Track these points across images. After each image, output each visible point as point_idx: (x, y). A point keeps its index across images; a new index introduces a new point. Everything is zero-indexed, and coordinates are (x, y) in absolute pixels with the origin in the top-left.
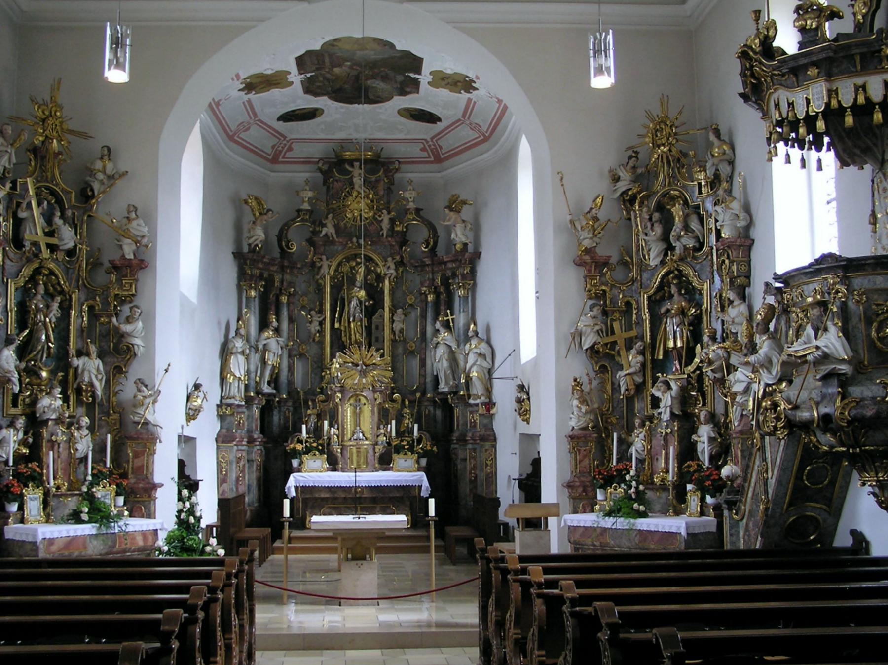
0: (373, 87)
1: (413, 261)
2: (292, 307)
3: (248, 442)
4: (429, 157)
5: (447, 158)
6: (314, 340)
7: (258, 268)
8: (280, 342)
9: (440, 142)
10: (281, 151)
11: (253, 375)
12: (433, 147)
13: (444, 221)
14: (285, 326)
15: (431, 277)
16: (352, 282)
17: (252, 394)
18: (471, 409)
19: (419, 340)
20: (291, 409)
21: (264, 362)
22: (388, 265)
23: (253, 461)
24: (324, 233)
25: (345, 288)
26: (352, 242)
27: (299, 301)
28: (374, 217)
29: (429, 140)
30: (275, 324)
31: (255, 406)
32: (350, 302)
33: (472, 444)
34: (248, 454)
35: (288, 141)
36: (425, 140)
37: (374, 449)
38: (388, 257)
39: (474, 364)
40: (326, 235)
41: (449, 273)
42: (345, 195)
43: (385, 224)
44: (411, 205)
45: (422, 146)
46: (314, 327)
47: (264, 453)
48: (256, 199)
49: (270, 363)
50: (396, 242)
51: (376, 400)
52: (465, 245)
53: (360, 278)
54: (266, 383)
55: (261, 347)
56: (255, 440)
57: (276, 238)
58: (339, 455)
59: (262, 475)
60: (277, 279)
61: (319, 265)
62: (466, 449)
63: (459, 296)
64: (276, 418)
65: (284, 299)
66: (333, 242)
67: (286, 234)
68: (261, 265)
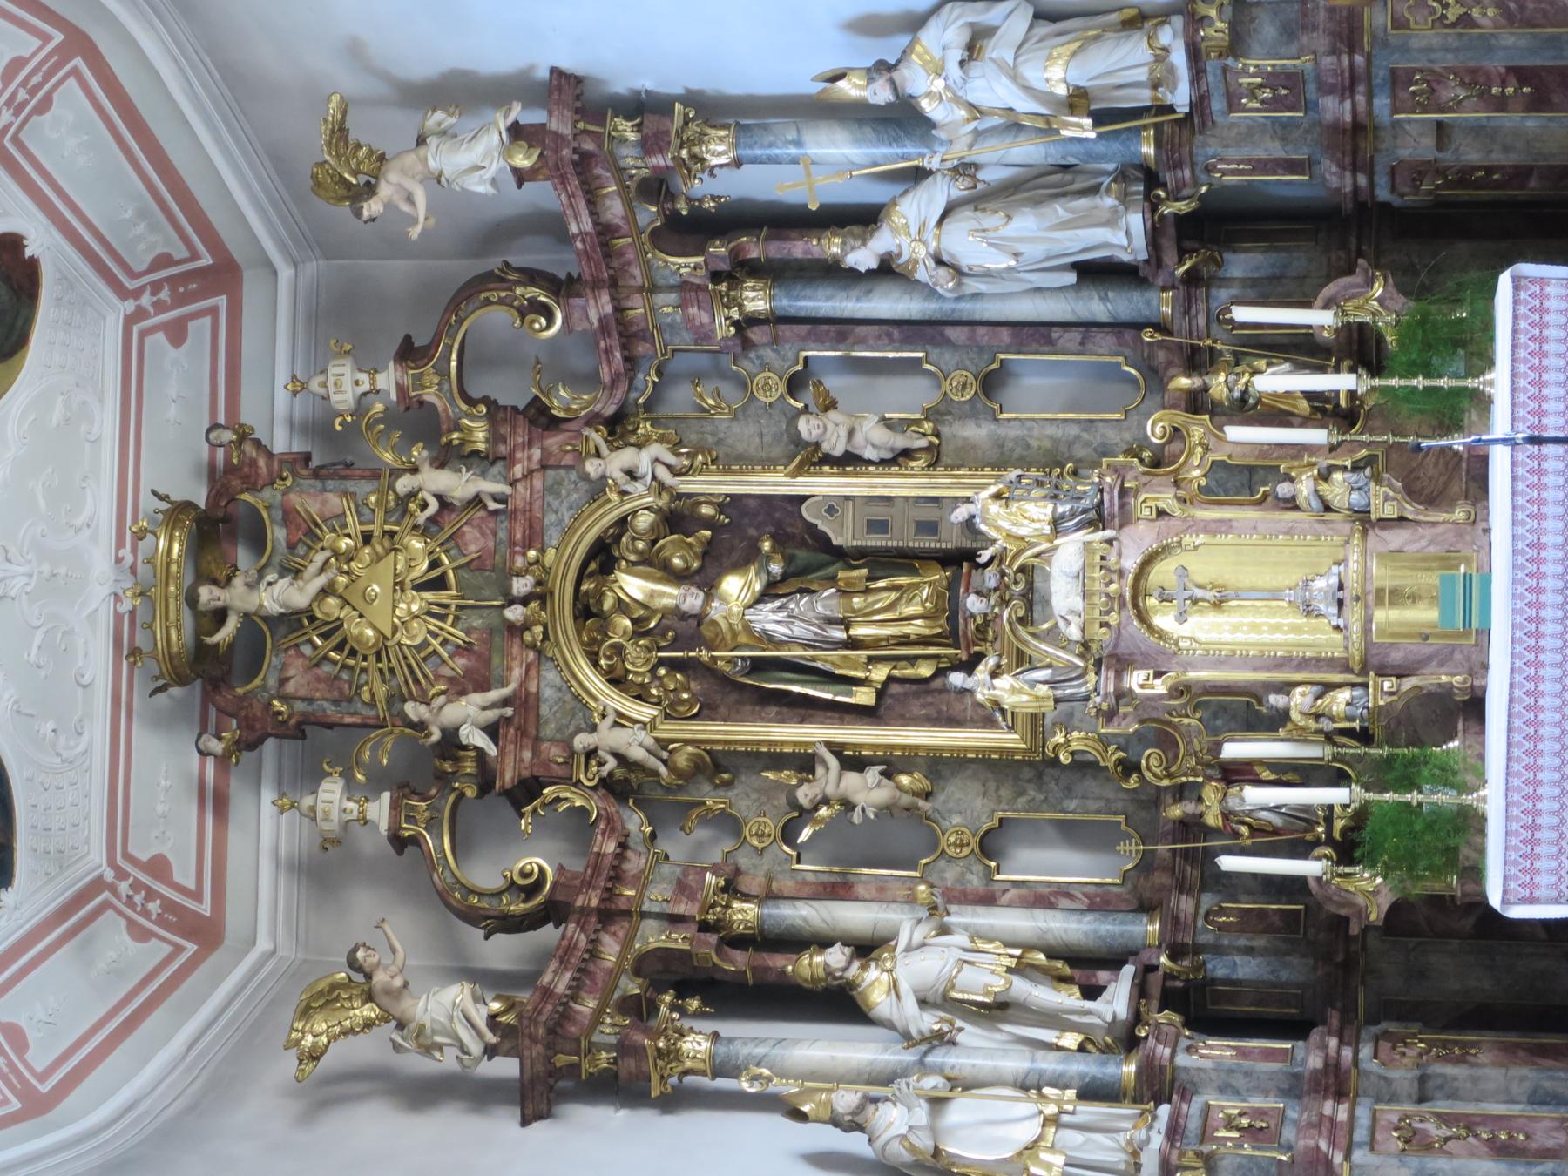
1: (605, 375)
2: (785, 884)
3: (1340, 1095)
4: (213, 312)
6: (927, 795)
7: (597, 1018)
8: (918, 937)
9: (140, 262)
10: (169, 905)
11: (1049, 1063)
12: (164, 295)
13: (415, 221)
14: (854, 916)
15: (673, 297)
16: (691, 628)
17: (1130, 1069)
18: (1217, 104)
19: (935, 353)
20: (1208, 900)
21: (997, 1010)
22: (618, 475)
23: (1423, 1079)
24: (480, 740)
25: (704, 655)
26: (526, 626)
27: (761, 853)
28: (424, 531)
29: (130, 306)
30: (836, 957)
31: (1182, 1060)
32: (769, 640)
33: (1370, 97)
34: (1393, 1098)
35: (121, 874)
36: (130, 321)
37: (1384, 523)
38: (585, 477)
39: (1015, 76)
40: (492, 730)
41: (648, 215)
42: (339, 648)
43: (459, 484)
44: (388, 379)
45: (160, 337)
46: (868, 790)
47: (1392, 1027)
48: (306, 1012)
49: (998, 984)
50: (530, 444)
51: (1161, 513)
52: (517, 132)
53: (670, 595)
54: (1089, 1004)
55: (929, 1021)
56: (1333, 1068)
57: (500, 938)
58: (1408, 683)
59: (1488, 1037)
60: (653, 936)
61: (611, 763)
62: (1396, 124)
63: (738, 163)
64: (1247, 968)
65: (744, 913)
66: (524, 702)
67: (481, 894)
68: (588, 1005)
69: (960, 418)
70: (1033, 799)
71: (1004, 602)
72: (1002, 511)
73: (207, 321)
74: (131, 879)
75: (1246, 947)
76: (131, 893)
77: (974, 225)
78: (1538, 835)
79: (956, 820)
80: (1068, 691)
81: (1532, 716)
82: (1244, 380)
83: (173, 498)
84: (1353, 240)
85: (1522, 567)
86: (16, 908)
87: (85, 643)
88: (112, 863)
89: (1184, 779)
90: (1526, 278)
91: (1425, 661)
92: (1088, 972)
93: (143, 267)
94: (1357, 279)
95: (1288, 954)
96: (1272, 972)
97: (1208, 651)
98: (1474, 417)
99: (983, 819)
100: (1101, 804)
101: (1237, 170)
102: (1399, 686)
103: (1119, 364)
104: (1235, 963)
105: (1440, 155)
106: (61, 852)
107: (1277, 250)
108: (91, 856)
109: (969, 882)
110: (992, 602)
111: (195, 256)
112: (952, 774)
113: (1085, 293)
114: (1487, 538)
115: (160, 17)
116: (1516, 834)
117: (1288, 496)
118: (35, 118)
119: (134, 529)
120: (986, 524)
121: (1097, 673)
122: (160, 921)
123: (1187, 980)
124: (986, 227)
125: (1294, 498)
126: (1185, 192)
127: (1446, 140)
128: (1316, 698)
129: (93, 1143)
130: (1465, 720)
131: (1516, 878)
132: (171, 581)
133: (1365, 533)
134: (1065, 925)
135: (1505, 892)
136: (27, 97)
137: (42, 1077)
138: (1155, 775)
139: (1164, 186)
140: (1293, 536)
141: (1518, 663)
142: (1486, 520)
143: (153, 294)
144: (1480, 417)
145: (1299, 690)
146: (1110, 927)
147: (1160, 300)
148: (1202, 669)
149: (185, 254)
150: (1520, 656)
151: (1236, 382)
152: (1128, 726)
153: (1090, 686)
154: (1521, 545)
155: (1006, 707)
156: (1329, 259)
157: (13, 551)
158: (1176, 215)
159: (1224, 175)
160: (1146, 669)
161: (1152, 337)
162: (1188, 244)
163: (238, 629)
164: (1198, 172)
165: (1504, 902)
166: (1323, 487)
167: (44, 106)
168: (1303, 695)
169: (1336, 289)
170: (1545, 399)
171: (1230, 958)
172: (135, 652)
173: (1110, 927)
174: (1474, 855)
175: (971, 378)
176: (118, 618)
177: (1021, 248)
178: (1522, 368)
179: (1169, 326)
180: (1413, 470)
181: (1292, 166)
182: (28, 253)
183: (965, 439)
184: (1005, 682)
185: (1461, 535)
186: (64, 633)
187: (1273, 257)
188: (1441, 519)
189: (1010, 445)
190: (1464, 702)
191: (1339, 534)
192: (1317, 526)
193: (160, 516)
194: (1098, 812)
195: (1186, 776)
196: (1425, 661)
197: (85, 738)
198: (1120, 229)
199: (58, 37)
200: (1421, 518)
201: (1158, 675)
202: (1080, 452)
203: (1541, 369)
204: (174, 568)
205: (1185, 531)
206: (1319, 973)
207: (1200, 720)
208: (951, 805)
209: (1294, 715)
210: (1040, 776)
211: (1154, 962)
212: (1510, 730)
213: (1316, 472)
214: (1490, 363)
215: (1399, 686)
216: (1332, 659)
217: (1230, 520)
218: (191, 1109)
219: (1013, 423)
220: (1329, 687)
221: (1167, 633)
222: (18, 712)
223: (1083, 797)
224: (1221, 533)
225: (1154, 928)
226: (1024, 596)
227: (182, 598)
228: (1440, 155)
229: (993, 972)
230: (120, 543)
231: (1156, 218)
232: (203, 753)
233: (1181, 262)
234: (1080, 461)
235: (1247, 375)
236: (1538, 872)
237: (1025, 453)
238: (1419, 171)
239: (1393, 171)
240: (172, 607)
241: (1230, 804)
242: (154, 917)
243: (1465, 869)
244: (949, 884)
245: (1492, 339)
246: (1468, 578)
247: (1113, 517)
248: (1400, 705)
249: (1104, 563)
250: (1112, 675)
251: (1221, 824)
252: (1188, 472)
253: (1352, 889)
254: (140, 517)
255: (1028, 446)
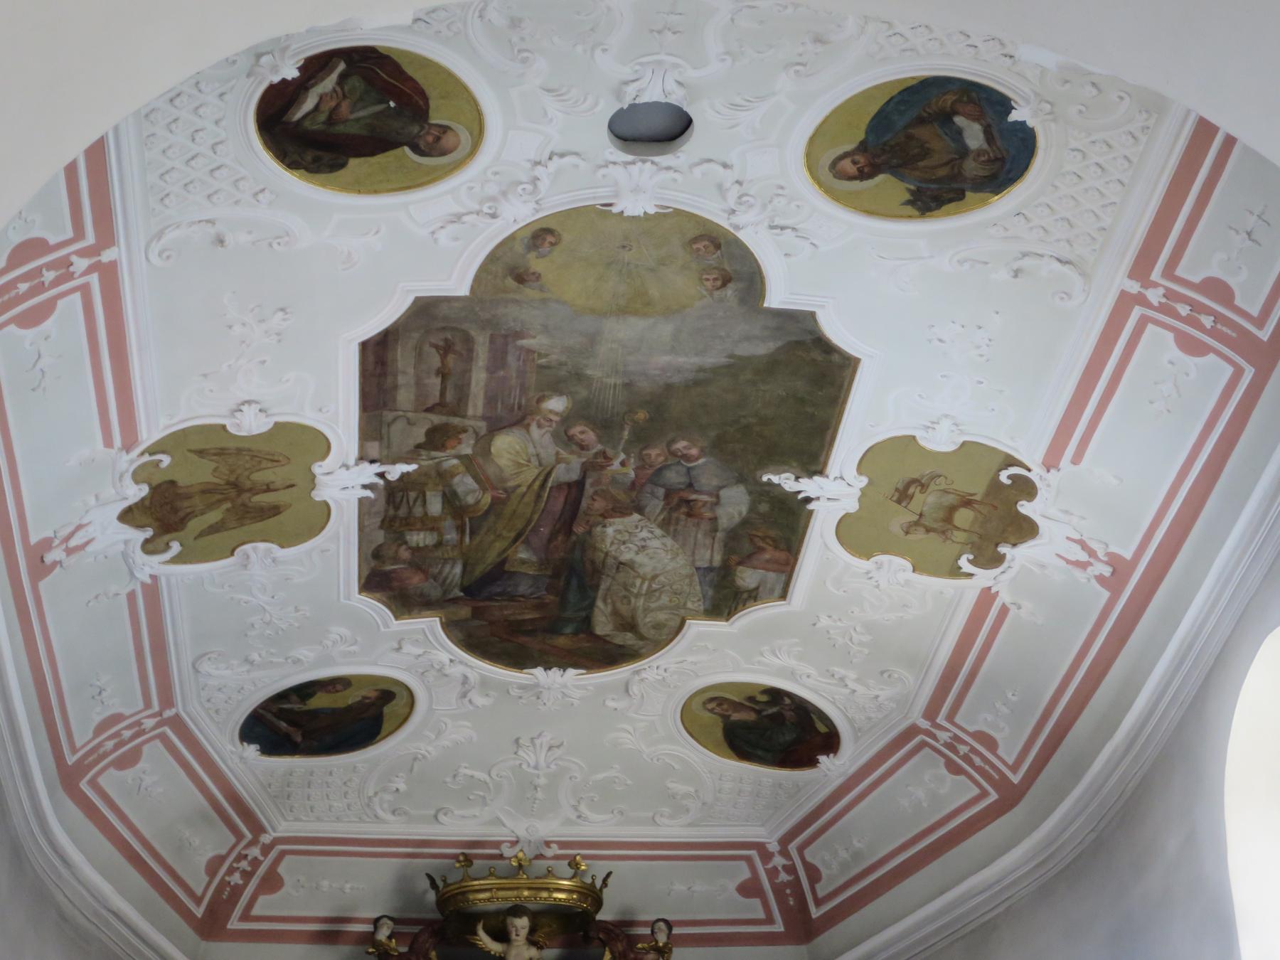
0: (620, 565)
4: (769, 920)
5: (832, 918)
10: (237, 891)
12: (784, 877)
29: (774, 847)
35: (266, 850)
36: (760, 847)
45: (745, 874)
73: (761, 915)
74: (261, 858)
76: (249, 858)
83: (605, 890)
86: (241, 758)
87: (475, 816)
88: (277, 841)
93: (809, 859)
106: (289, 797)
108: (284, 823)
111: (819, 903)
115: (1038, 866)
118: (942, 760)
119: (578, 858)
122: (223, 884)
129: (36, 830)
132: (533, 892)
136: (962, 753)
137: (93, 783)
143: (784, 867)
149: (821, 894)
157: (558, 752)
163: (489, 952)
167: (954, 768)
172: (468, 860)
176: (497, 844)
182: (822, 758)
186: (484, 798)
193: (589, 881)
197: (389, 817)
199: (1015, 779)
204: (545, 894)
218: (63, 917)
222: (415, 759)
227: (518, 902)
230: (563, 845)
232: (376, 922)
240: (509, 893)
242: (227, 878)
254: (589, 862)
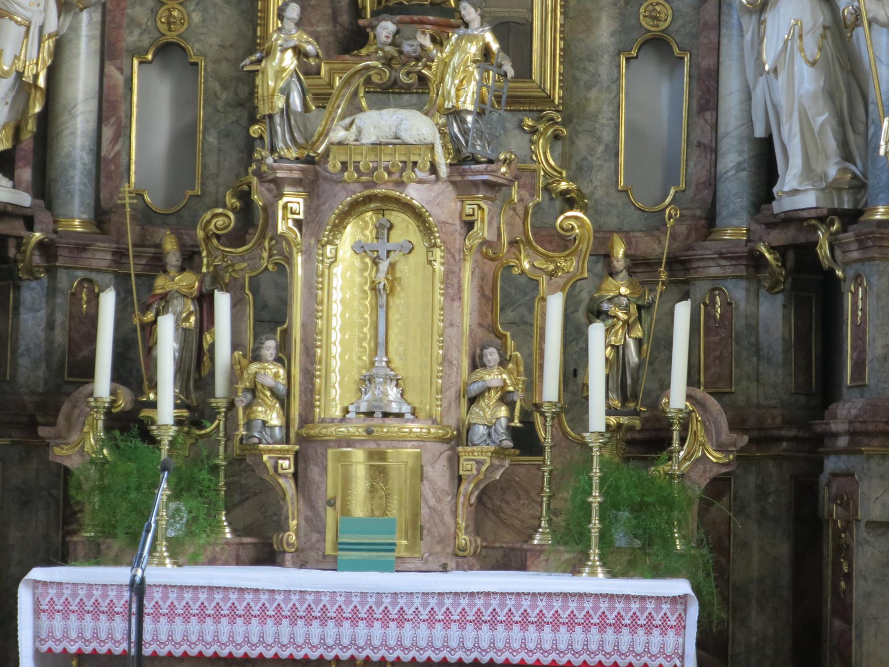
51: (469, 225)
58: (288, 485)
69: (621, 14)
70: (218, 98)
71: (388, 62)
72: (470, 56)
75: (54, 321)
77: (808, 25)
78: (103, 617)
79: (196, 17)
80: (279, 129)
81: (225, 612)
82: (621, 315)
84: (792, 433)
85: (379, 603)
89: (204, 254)
90: (685, 610)
91: (311, 504)
92: (30, 156)
94: (726, 435)
95: (49, 366)
96: (28, 350)
97: (322, 275)
98: (566, 556)
99: (197, 46)
100: (212, 167)
101: (857, 307)
102: (285, 476)
103: (677, 184)
104: (38, 311)
105: (862, 525)
107: (786, 352)
109: (131, 33)
110: (388, 49)
112: (243, 12)
113: (746, 147)
114: (436, 568)
116: (105, 596)
117: (485, 360)
120: (457, 40)
121: (297, 159)
123: (16, 261)
124: (805, 38)
125: (484, 366)
126: (838, 252)
127: (880, 531)
128: (271, 389)
130: (255, 544)
131: (60, 595)
133: (443, 440)
134: (79, 132)
135: (45, 584)
138: (209, 222)
139: (844, 229)
140: (441, 364)
141: (279, 598)
142: (458, 568)
144: (567, 561)
145: (282, 372)
146: (77, 179)
147: (738, 227)
148: (305, 270)
150: (287, 600)
151: (619, 306)
152: (260, 193)
153: (285, 153)
154: (402, 601)
155: (263, 64)
156: (775, 407)
158: (816, 243)
159: (853, 294)
160: (305, 212)
161: (670, 217)
162: (791, 256)
164: (856, 266)
165: (36, 582)
166: (494, 396)
168: (276, 375)
169: (715, 413)
170: (555, 628)
171: (44, 305)
173: (77, 179)
174: (112, 554)
175: (664, 26)
177: (782, 77)
178: (588, 605)
179: (713, 236)
180: (527, 492)
181: (859, 366)
183: (598, 20)
184: (289, 61)
185: (442, 540)
187: (779, 347)
188: (460, 521)
189: (591, 69)
190: (271, 545)
191: (446, 411)
192: (453, 390)
194: (204, 166)
195: (208, 256)
196: (311, 504)
198: (801, 184)
200: (461, 499)
201: (298, 223)
202: (583, 143)
203: (587, 625)
205: (448, 251)
206: (27, 398)
207: (266, 268)
208: (211, 11)
209: (254, 367)
210: (241, 104)
211: (37, 226)
212: (211, 588)
213: (511, 389)
214: (612, 574)
215: (285, 476)
216: (313, 406)
217: (460, 299)
219: (616, 71)
220: (284, 401)
221: (341, 233)
223: (220, 150)
224: (446, 288)
225: (77, 226)
226: (395, 82)
228: (862, 525)
229: (17, 57)
231: (813, 222)
233: (772, 249)
234: (572, 143)
235: (626, 317)
236: (66, 618)
237: (582, 83)
238: (848, 501)
239: (849, 475)
241: (176, 302)
243: (99, 545)
244: (129, 11)
245: (643, 576)
246: (390, 547)
247: (462, 174)
248: (265, 477)
249: (410, 165)
250: (296, 175)
251: (158, 292)
252: (527, 256)
253: (85, 430)
255: (589, 87)
